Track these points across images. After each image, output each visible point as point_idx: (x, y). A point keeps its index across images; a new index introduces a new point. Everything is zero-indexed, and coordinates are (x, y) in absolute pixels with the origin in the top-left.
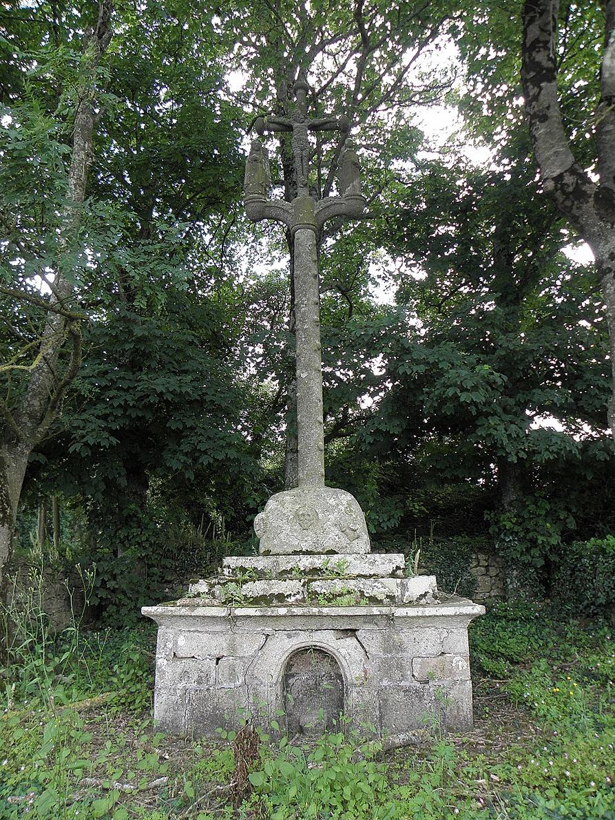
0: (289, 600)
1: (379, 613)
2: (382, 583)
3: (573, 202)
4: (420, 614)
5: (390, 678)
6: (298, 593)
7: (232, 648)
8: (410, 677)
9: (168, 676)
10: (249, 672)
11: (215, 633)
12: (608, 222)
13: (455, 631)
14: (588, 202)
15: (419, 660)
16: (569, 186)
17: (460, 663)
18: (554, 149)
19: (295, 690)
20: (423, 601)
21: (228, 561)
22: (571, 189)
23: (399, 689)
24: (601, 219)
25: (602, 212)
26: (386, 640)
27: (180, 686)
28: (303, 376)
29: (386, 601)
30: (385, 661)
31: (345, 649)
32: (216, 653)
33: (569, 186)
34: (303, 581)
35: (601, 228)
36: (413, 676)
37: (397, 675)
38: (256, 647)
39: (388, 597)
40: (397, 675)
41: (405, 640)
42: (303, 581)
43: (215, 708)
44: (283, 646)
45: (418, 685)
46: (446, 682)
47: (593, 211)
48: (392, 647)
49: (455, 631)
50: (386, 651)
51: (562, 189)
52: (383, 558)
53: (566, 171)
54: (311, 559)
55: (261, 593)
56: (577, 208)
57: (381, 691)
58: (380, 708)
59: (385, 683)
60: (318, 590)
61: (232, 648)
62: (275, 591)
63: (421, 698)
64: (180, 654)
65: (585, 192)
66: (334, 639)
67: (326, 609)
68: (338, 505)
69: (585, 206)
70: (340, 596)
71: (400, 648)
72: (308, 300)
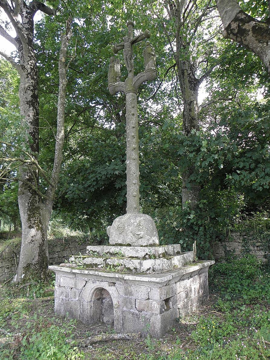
0: (99, 266)
1: (118, 277)
2: (133, 262)
3: (241, 38)
4: (134, 279)
5: (127, 307)
6: (102, 264)
7: (75, 285)
8: (134, 308)
9: (58, 293)
10: (81, 295)
11: (71, 278)
12: (264, 42)
13: (154, 289)
14: (248, 35)
15: (139, 301)
16: (235, 30)
17: (155, 305)
18: (225, 10)
19: (105, 305)
20: (148, 272)
21: (89, 248)
22: (236, 31)
23: (130, 312)
24: (259, 42)
25: (259, 37)
26: (126, 289)
27: (61, 297)
28: (128, 163)
29: (134, 270)
30: (125, 299)
31: (111, 290)
32: (71, 286)
33: (235, 30)
34: (104, 258)
35: (261, 47)
36: (136, 308)
37: (129, 306)
38: (83, 286)
39: (134, 268)
40: (129, 306)
41: (133, 290)
42: (104, 258)
43: (71, 308)
44: (92, 286)
45: (137, 312)
46: (149, 313)
47: (253, 39)
48: (128, 293)
49: (154, 289)
50: (126, 294)
51: (232, 32)
52: (141, 249)
53: (232, 22)
54: (115, 248)
55: (90, 263)
56: (245, 40)
57: (123, 312)
58: (123, 320)
59: (125, 309)
60: (109, 263)
61: (75, 285)
62: (94, 262)
63: (138, 318)
64: (61, 285)
65: (245, 29)
66: (108, 286)
67: (141, 267)
68: (134, 223)
69: (248, 38)
70: (117, 266)
71: (131, 294)
72: (130, 126)
